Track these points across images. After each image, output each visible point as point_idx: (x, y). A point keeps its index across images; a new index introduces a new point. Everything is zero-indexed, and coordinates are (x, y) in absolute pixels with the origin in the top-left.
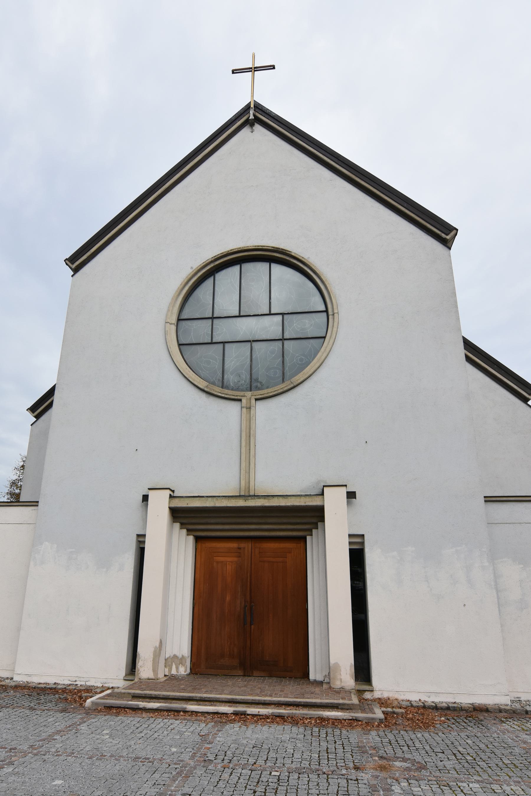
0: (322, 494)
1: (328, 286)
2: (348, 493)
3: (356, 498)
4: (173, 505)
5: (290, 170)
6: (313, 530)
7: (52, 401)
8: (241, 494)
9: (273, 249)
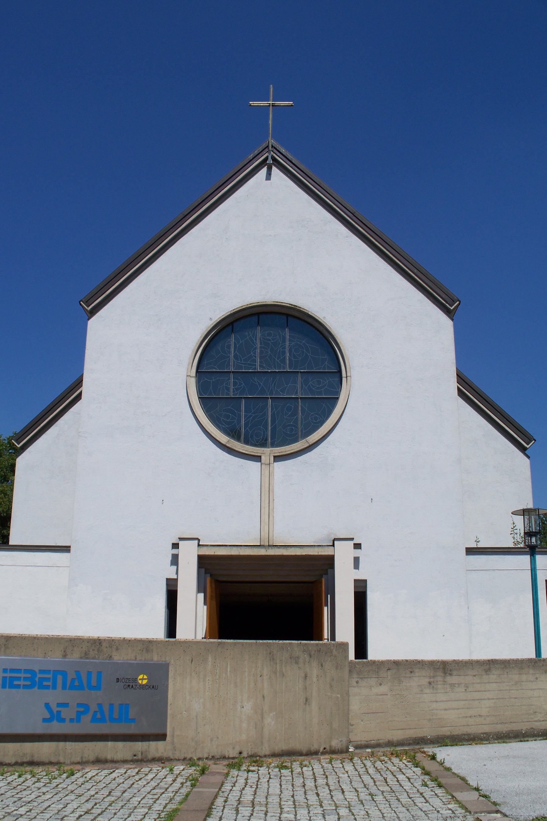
0: (333, 545)
1: (342, 348)
2: (354, 544)
3: (361, 549)
4: (201, 553)
5: (308, 221)
6: (323, 576)
7: (80, 394)
8: (261, 544)
9: (291, 306)
